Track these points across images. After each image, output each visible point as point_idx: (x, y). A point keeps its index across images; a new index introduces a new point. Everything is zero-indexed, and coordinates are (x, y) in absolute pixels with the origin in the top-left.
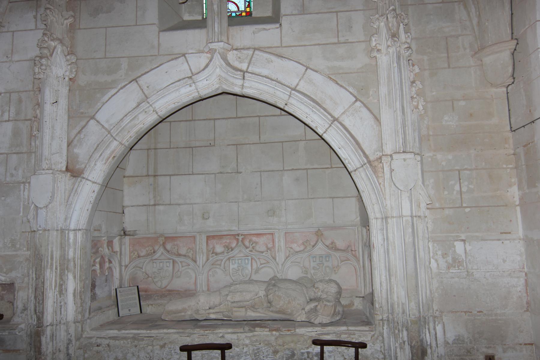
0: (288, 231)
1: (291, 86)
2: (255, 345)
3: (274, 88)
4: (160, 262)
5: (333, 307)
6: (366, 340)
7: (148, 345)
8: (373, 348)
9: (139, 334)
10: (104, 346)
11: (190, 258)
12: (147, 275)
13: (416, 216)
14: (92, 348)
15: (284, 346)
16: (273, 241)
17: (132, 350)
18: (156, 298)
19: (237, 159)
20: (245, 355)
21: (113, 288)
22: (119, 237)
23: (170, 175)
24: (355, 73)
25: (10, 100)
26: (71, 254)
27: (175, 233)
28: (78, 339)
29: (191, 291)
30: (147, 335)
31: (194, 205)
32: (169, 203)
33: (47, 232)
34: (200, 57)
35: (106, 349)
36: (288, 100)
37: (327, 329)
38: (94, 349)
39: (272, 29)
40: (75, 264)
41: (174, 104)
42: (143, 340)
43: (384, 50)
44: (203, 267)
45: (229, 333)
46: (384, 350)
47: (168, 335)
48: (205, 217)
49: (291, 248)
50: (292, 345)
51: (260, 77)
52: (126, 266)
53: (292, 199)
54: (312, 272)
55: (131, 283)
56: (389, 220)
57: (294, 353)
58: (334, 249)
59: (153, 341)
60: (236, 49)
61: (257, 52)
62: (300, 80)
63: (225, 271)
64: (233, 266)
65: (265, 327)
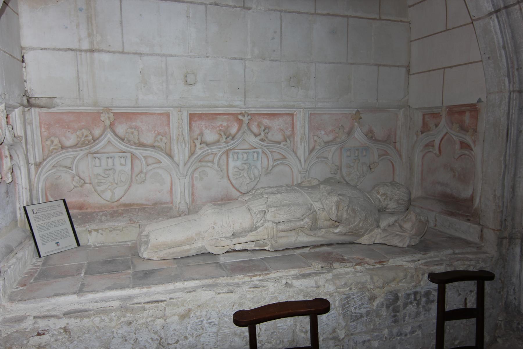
0: (315, 112)
4: (108, 158)
7: (156, 318)
9: (130, 298)
10: (55, 333)
11: (162, 150)
12: (82, 181)
14: (25, 342)
17: (120, 331)
18: (104, 218)
21: (19, 206)
27: (134, 107)
29: (165, 203)
31: (168, 58)
32: (121, 50)
35: (60, 337)
37: (429, 255)
38: (31, 342)
52: (38, 165)
55: (48, 194)
59: (165, 309)
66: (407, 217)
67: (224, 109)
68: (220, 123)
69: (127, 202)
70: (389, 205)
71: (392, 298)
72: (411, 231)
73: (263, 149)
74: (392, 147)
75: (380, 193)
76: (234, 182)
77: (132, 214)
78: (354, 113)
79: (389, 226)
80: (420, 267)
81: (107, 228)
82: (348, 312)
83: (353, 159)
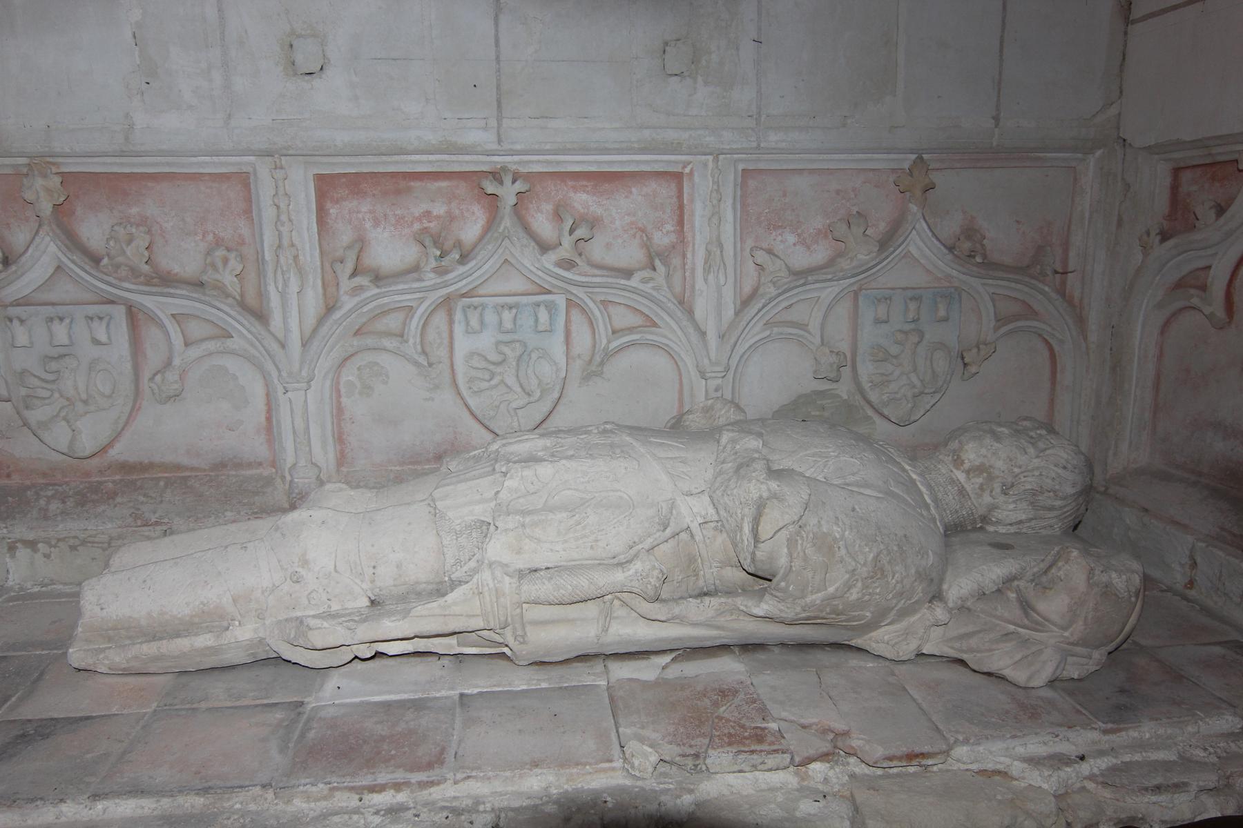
0: (761, 166)
18: (55, 506)
29: (250, 465)
37: (1134, 734)
66: (1053, 570)
67: (431, 157)
68: (424, 206)
69: (132, 458)
70: (997, 508)
72: (1065, 629)
73: (572, 293)
74: (1047, 289)
75: (967, 465)
76: (472, 402)
77: (145, 495)
78: (906, 166)
79: (982, 595)
80: (1083, 788)
81: (62, 536)
83: (900, 331)
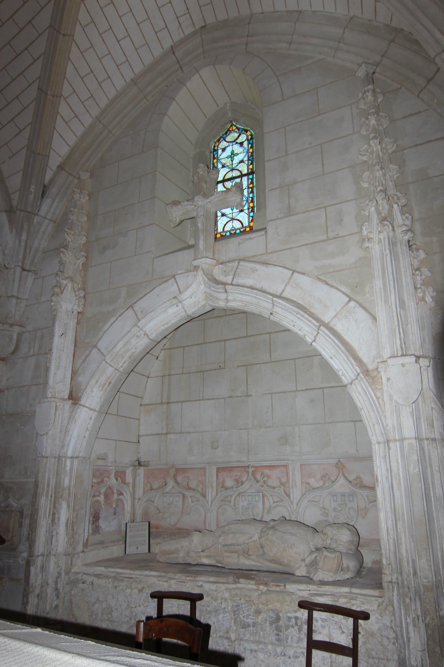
0: (304, 463)
1: (276, 293)
2: (235, 601)
3: (256, 297)
5: (336, 559)
6: (370, 608)
8: (380, 621)
10: (88, 583)
13: (427, 439)
15: (267, 606)
16: (287, 474)
19: (247, 381)
20: (223, 612)
21: (124, 522)
22: (132, 468)
23: (182, 402)
24: (347, 269)
25: (36, 337)
26: (66, 482)
28: (67, 573)
30: (128, 576)
33: (45, 459)
34: (188, 276)
35: (89, 587)
36: (273, 308)
39: (257, 236)
40: (69, 493)
41: (163, 325)
42: (123, 580)
43: (376, 239)
44: (212, 503)
45: (210, 582)
46: (396, 626)
47: (147, 578)
48: (214, 446)
49: (308, 484)
50: (278, 605)
51: (241, 288)
52: (139, 499)
53: (307, 425)
54: (333, 514)
56: (391, 444)
57: (279, 616)
58: (358, 485)
59: (132, 583)
60: (222, 263)
61: (242, 263)
62: (286, 286)
63: (235, 508)
64: (243, 503)
65: (252, 579)
71: (275, 616)
82: (238, 618)
